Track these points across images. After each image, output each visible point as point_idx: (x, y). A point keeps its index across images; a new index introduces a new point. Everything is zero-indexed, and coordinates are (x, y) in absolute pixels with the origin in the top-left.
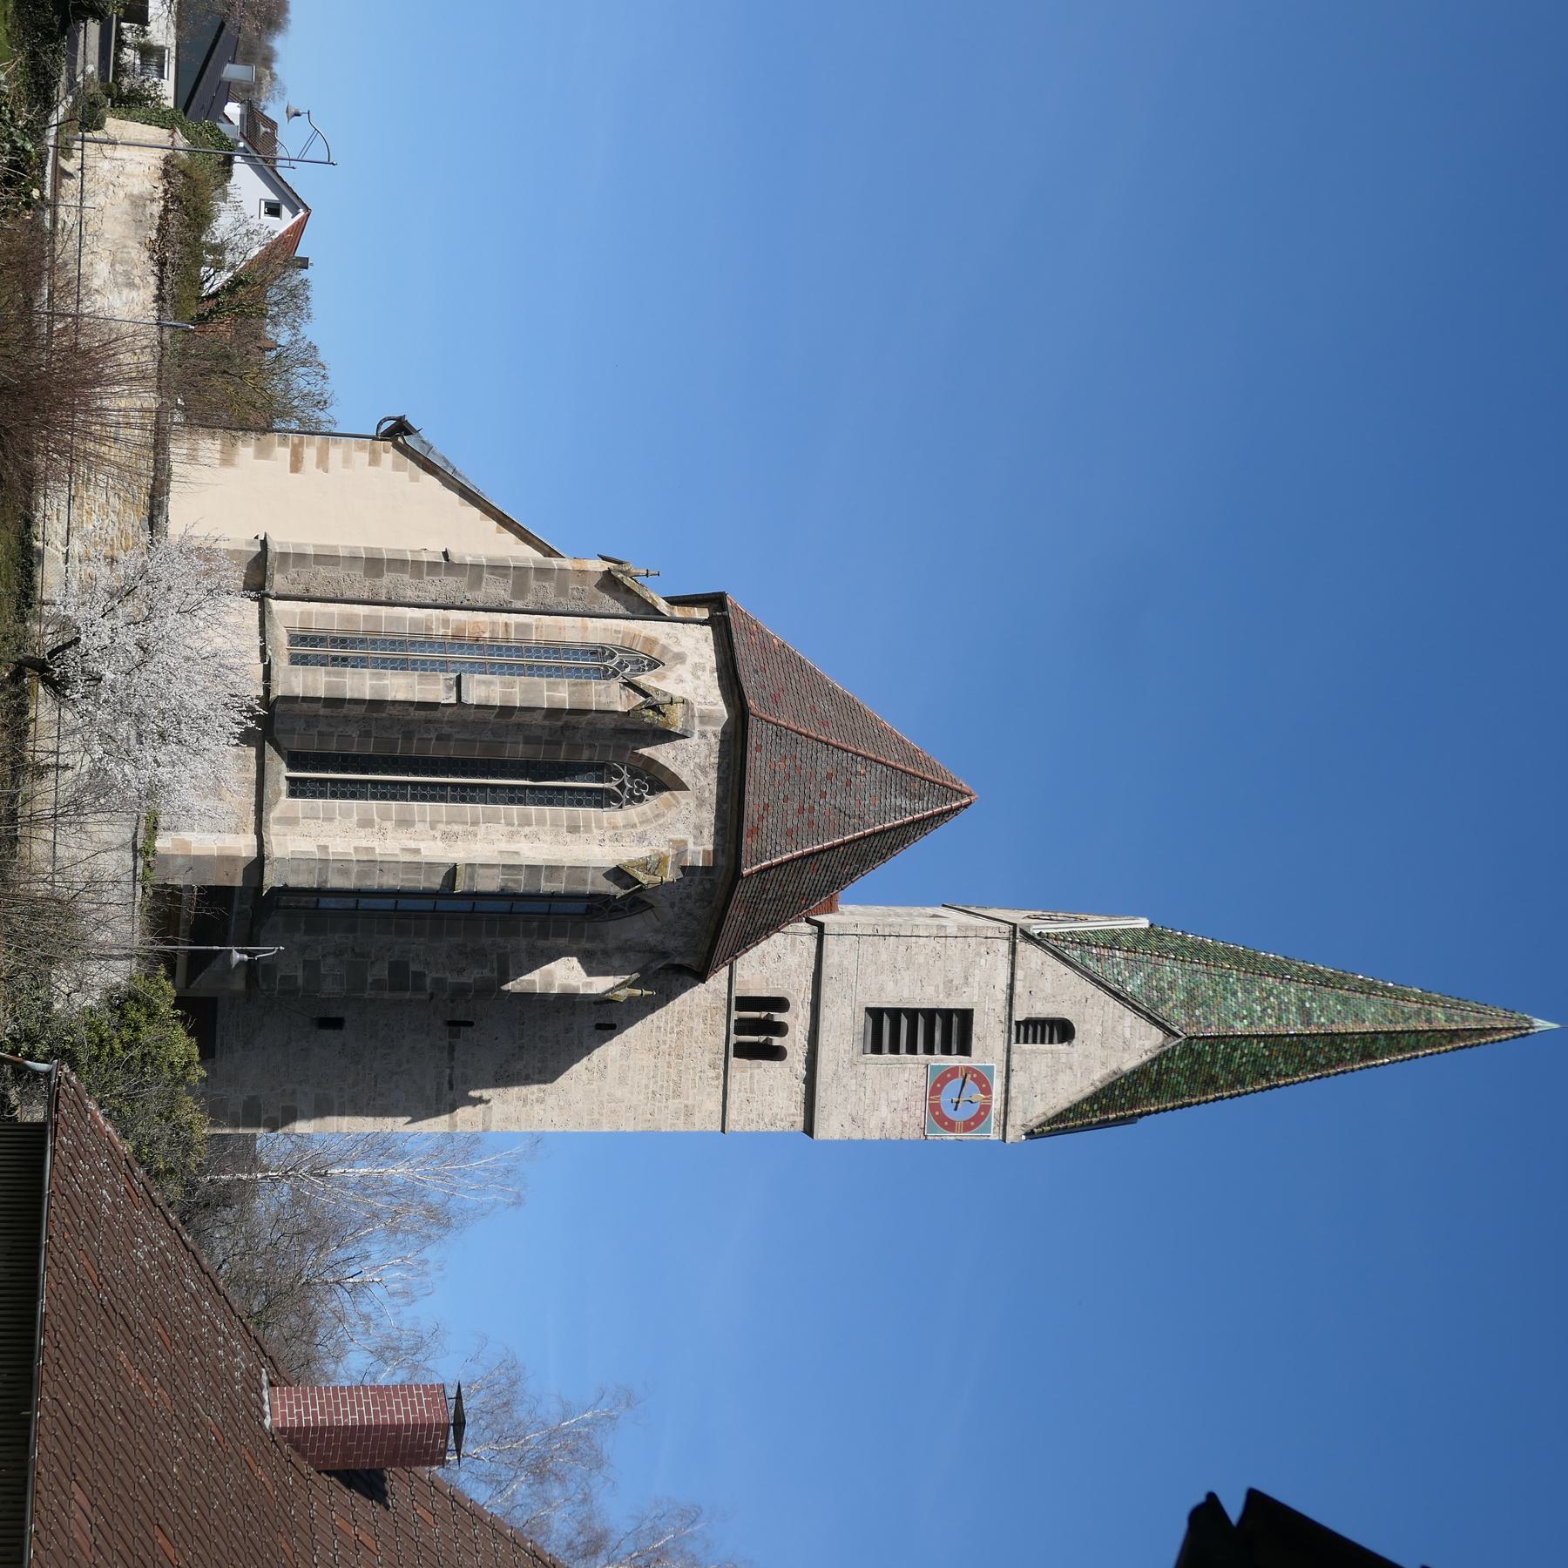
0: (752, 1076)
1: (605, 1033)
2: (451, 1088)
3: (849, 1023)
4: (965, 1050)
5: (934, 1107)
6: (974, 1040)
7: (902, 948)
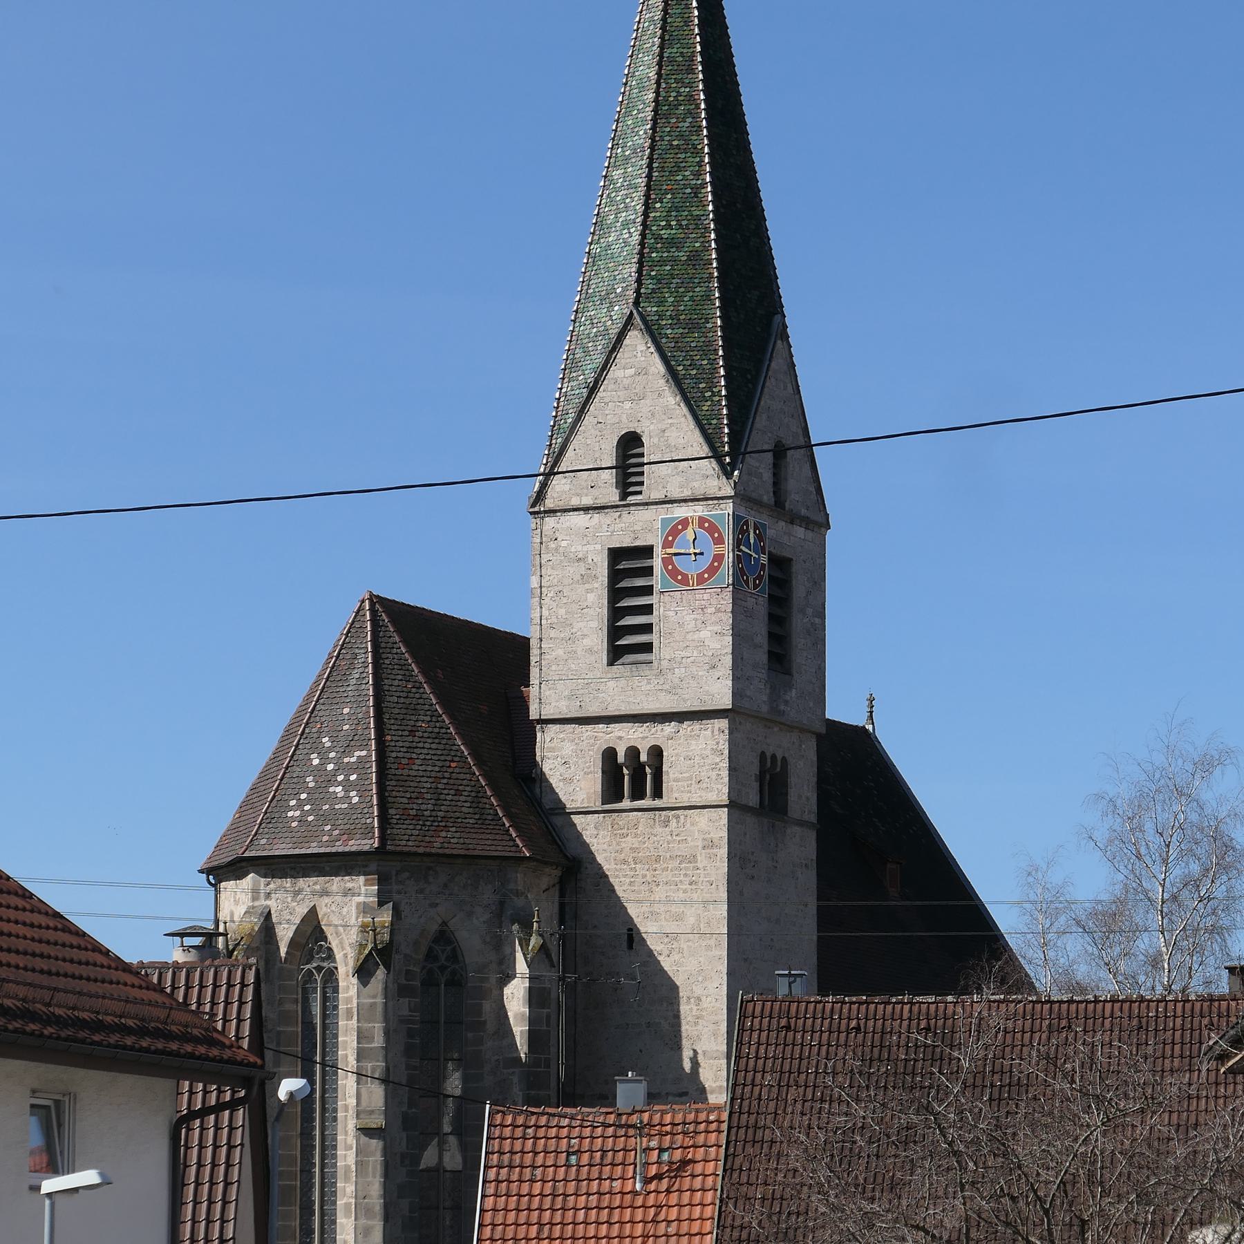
1: (636, 939)
3: (623, 682)
4: (647, 551)
5: (701, 580)
6: (637, 543)
7: (553, 633)
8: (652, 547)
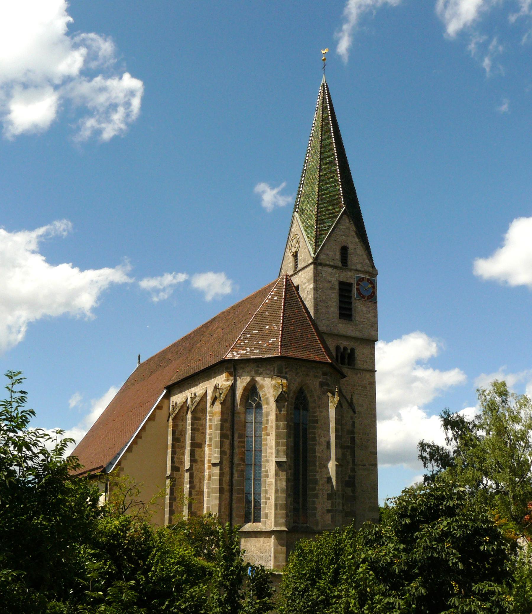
0: (360, 361)
2: (365, 465)
3: (344, 325)
6: (348, 281)
7: (321, 304)
8: (341, 283)
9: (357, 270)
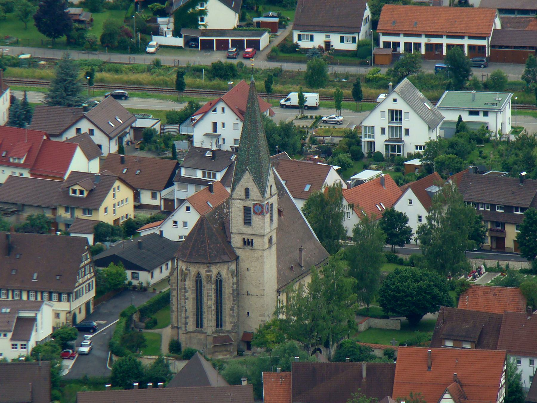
9: (254, 200)
